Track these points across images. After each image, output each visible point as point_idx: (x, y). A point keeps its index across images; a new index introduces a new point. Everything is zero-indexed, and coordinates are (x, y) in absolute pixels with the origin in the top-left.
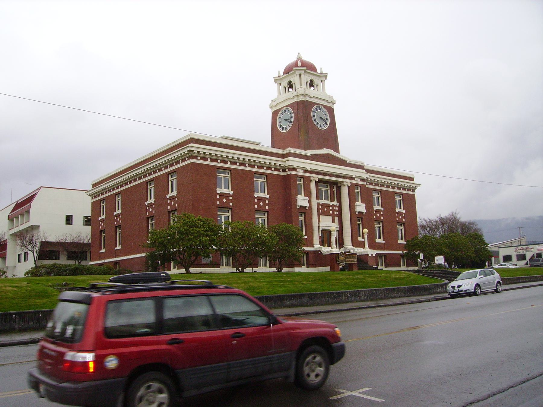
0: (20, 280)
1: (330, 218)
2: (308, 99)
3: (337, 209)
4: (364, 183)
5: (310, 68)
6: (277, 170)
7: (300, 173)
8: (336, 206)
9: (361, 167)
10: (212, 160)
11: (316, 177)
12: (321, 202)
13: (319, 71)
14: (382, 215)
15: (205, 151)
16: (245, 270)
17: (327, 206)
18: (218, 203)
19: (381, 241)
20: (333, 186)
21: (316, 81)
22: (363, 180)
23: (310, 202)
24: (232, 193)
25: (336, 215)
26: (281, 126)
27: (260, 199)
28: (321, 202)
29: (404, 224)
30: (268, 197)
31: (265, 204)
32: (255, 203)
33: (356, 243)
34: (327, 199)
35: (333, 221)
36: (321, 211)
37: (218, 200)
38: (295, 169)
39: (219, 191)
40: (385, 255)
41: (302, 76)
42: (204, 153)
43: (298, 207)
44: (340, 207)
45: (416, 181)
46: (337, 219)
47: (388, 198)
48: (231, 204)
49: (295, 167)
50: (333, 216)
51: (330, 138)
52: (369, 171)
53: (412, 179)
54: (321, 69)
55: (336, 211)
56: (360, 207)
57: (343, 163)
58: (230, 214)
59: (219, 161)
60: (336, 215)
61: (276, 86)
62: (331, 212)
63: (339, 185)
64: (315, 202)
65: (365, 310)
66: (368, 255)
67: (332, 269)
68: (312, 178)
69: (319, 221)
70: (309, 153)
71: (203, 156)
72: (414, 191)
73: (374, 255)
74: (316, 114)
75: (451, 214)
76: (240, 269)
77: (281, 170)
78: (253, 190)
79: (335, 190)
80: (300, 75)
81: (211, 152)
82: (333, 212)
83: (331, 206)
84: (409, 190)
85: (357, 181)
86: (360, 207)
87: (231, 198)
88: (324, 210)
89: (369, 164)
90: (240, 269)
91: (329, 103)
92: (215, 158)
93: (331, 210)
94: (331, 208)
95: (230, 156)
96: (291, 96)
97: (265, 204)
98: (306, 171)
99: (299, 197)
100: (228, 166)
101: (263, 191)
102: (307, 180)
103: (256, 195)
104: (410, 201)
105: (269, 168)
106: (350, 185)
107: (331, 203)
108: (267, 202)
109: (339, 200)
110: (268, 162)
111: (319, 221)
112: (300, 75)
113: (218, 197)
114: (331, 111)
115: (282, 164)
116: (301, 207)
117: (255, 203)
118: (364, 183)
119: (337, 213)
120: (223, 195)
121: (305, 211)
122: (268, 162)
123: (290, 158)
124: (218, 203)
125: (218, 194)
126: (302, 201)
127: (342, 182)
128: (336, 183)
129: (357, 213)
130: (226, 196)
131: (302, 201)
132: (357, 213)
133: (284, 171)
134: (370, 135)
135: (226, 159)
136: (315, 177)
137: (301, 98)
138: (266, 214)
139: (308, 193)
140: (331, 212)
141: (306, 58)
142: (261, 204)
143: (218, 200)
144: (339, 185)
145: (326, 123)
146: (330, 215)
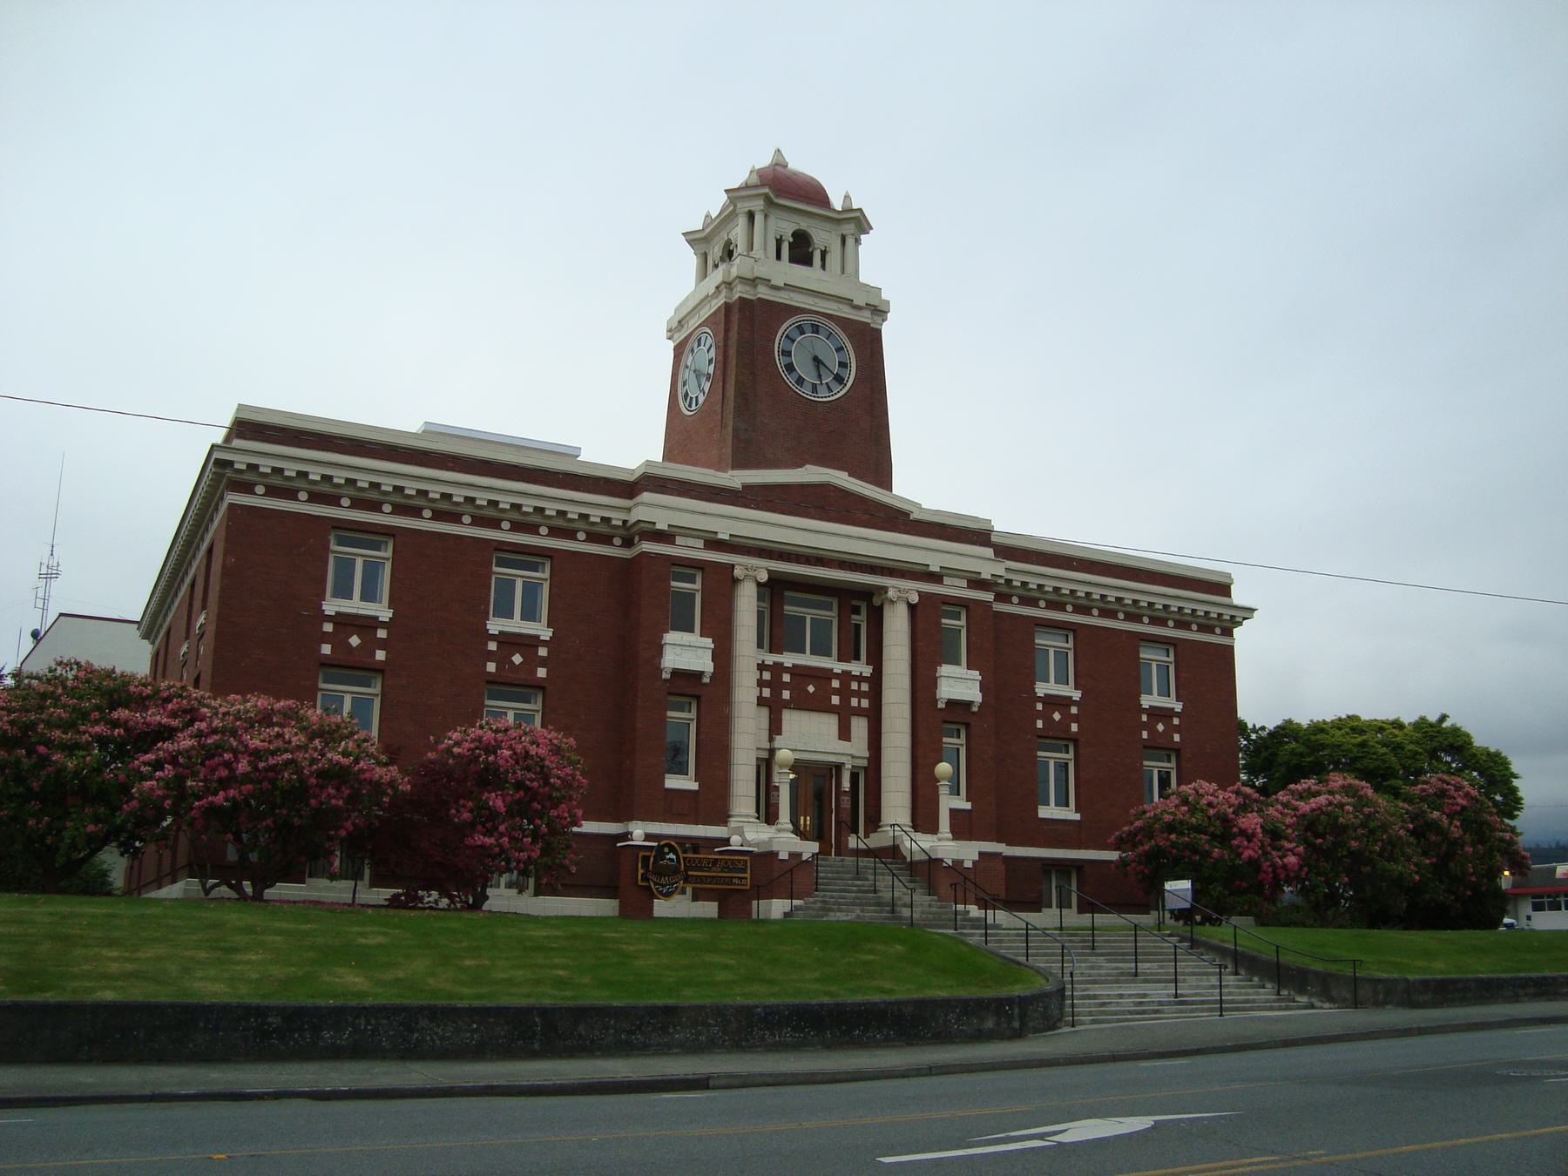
0: (776, 922)
1: (830, 723)
2: (764, 293)
3: (865, 687)
4: (988, 596)
5: (810, 194)
8: (860, 679)
9: (978, 535)
10: (478, 521)
11: (762, 569)
12: (789, 659)
14: (1177, 729)
15: (1137, 597)
16: (269, 893)
17: (824, 676)
18: (1040, 724)
19: (1070, 814)
21: (821, 236)
22: (977, 583)
24: (546, 634)
25: (859, 712)
26: (686, 395)
27: (1158, 714)
28: (789, 659)
29: (1178, 751)
30: (1178, 707)
32: (490, 656)
33: (924, 818)
34: (820, 649)
35: (845, 734)
36: (786, 695)
37: (1144, 726)
38: (666, 537)
39: (1041, 689)
40: (1079, 865)
41: (759, 218)
42: (1057, 589)
43: (666, 676)
44: (876, 680)
45: (1238, 597)
46: (859, 727)
47: (1107, 659)
48: (380, 655)
49: (935, 568)
50: (844, 717)
51: (860, 428)
52: (1010, 551)
53: (1223, 589)
54: (847, 197)
55: (859, 694)
56: (959, 683)
57: (898, 519)
58: (1071, 755)
59: (1095, 612)
60: (859, 712)
61: (690, 259)
62: (835, 700)
63: (876, 601)
64: (748, 654)
65: (104, 1107)
66: (774, 854)
67: (625, 913)
68: (738, 572)
70: (736, 478)
71: (1053, 597)
72: (1228, 632)
73: (968, 864)
76: (249, 889)
77: (617, 541)
78: (1136, 685)
79: (861, 619)
80: (751, 216)
81: (607, 514)
82: (845, 700)
83: (837, 676)
84: (1206, 628)
85: (954, 588)
86: (959, 683)
87: (1176, 721)
88: (788, 693)
89: (1008, 522)
90: (249, 889)
91: (858, 308)
92: (1085, 602)
94: (835, 684)
95: (266, 466)
97: (1170, 729)
98: (713, 544)
99: (945, 670)
100: (543, 541)
101: (1062, 679)
102: (722, 583)
103: (1041, 689)
104: (1209, 670)
105: (1182, 625)
106: (915, 599)
107: (839, 667)
108: (1074, 710)
109: (876, 658)
110: (1128, 598)
112: (751, 216)
113: (1039, 707)
114: (868, 343)
115: (617, 518)
116: (676, 673)
117: (490, 656)
118: (988, 596)
119: (865, 703)
120: (1053, 702)
122: (1049, 585)
123: (646, 496)
124: (1040, 724)
125: (329, 618)
127: (884, 589)
128: (867, 593)
129: (941, 705)
130: (1062, 703)
132: (666, 676)
133: (628, 543)
135: (1164, 615)
137: (740, 291)
138: (1173, 759)
140: (835, 700)
141: (801, 163)
142: (1160, 727)
143: (1040, 715)
144: (876, 601)
145: (839, 379)
146: (830, 709)
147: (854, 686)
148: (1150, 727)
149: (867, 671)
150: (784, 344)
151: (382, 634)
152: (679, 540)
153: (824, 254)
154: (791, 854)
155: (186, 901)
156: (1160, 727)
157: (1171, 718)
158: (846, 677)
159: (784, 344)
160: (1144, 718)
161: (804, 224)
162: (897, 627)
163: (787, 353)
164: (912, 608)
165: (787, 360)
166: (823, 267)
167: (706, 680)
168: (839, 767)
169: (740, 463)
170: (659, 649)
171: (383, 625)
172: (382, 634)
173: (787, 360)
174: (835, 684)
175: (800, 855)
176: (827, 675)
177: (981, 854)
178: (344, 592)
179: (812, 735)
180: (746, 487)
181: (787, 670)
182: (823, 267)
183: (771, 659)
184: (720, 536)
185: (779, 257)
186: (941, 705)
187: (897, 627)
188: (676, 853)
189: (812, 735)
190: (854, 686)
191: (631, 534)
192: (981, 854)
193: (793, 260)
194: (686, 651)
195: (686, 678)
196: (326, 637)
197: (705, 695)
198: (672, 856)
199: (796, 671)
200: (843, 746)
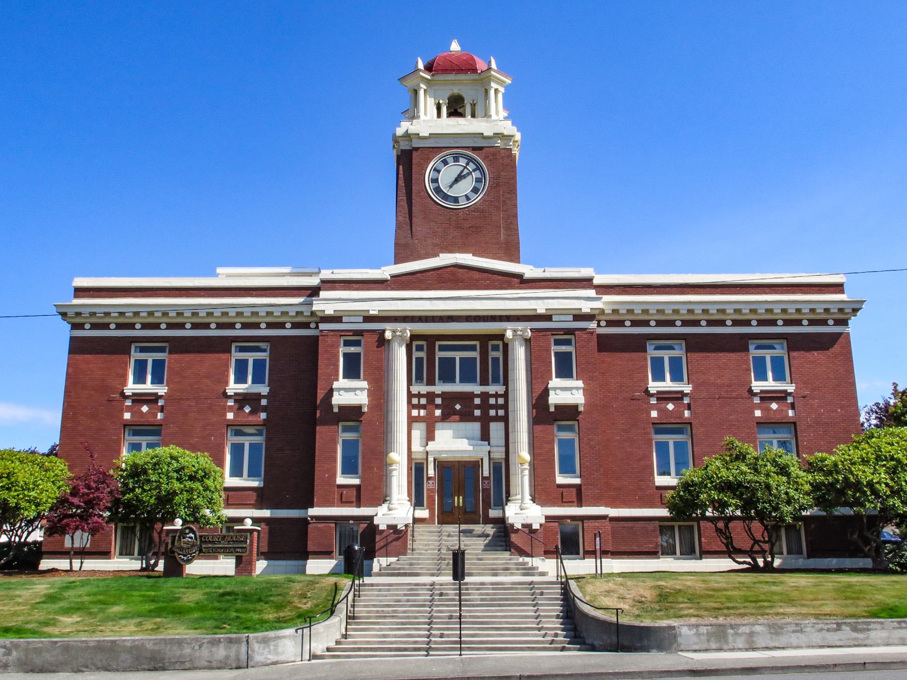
8: (496, 396)
25: (497, 419)
35: (485, 436)
55: (496, 407)
68: (388, 335)
70: (386, 272)
72: (844, 322)
82: (485, 413)
83: (477, 396)
91: (425, 138)
98: (368, 319)
140: (477, 413)
146: (474, 419)
147: (492, 401)
149: (501, 389)
150: (433, 175)
151: (264, 402)
152: (344, 319)
153: (473, 105)
154: (523, 525)
155: (132, 574)
157: (681, 399)
158: (485, 396)
159: (433, 175)
161: (456, 91)
162: (520, 355)
163: (435, 181)
164: (527, 341)
165: (436, 185)
167: (365, 409)
169: (398, 260)
171: (264, 397)
172: (264, 402)
173: (436, 185)
174: (477, 401)
175: (396, 526)
176: (471, 396)
177: (547, 517)
178: (762, 376)
179: (453, 442)
181: (438, 396)
183: (424, 389)
184: (371, 312)
185: (439, 115)
187: (520, 355)
188: (194, 532)
189: (453, 442)
190: (492, 401)
192: (547, 517)
193: (450, 115)
194: (349, 392)
195: (352, 413)
196: (653, 407)
198: (192, 535)
199: (444, 395)
200: (484, 448)
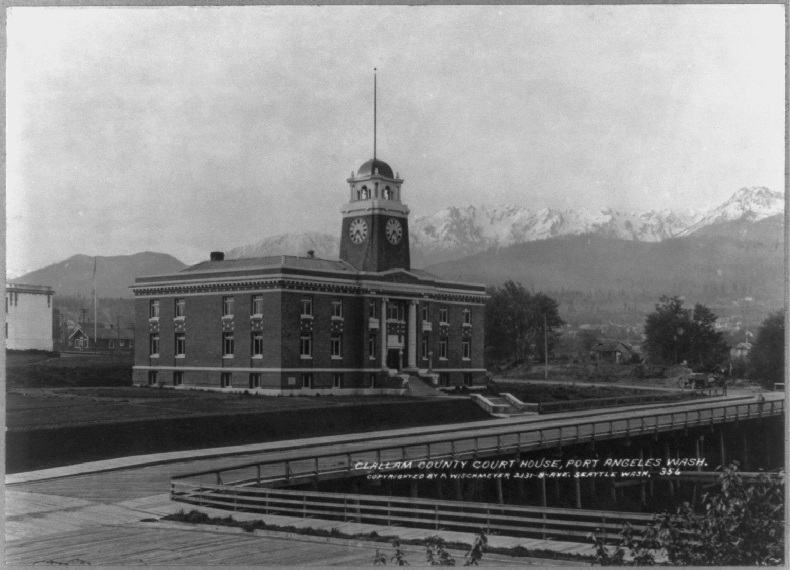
2: (383, 213)
6: (352, 292)
7: (373, 295)
8: (403, 325)
11: (386, 298)
13: (395, 177)
20: (401, 306)
22: (431, 296)
23: (380, 324)
24: (312, 318)
25: (403, 334)
31: (340, 327)
34: (395, 317)
35: (400, 341)
44: (407, 325)
46: (403, 338)
56: (427, 326)
57: (414, 281)
60: (403, 334)
62: (398, 331)
68: (383, 300)
69: (387, 341)
70: (382, 273)
74: (393, 228)
75: (401, 177)
79: (403, 308)
85: (426, 299)
87: (342, 324)
88: (392, 329)
93: (398, 329)
94: (398, 327)
96: (366, 206)
98: (378, 292)
102: (379, 302)
106: (418, 303)
107: (399, 322)
109: (407, 318)
111: (387, 341)
121: (375, 333)
126: (373, 324)
128: (405, 301)
131: (373, 324)
134: (403, 187)
136: (386, 298)
139: (378, 316)
140: (398, 331)
142: (337, 327)
148: (254, 325)
156: (337, 327)
160: (302, 323)
164: (417, 306)
166: (16, 304)
168: (784, 382)
170: (368, 322)
174: (398, 327)
180: (385, 276)
182: (16, 304)
186: (369, 330)
191: (358, 291)
197: (375, 333)
